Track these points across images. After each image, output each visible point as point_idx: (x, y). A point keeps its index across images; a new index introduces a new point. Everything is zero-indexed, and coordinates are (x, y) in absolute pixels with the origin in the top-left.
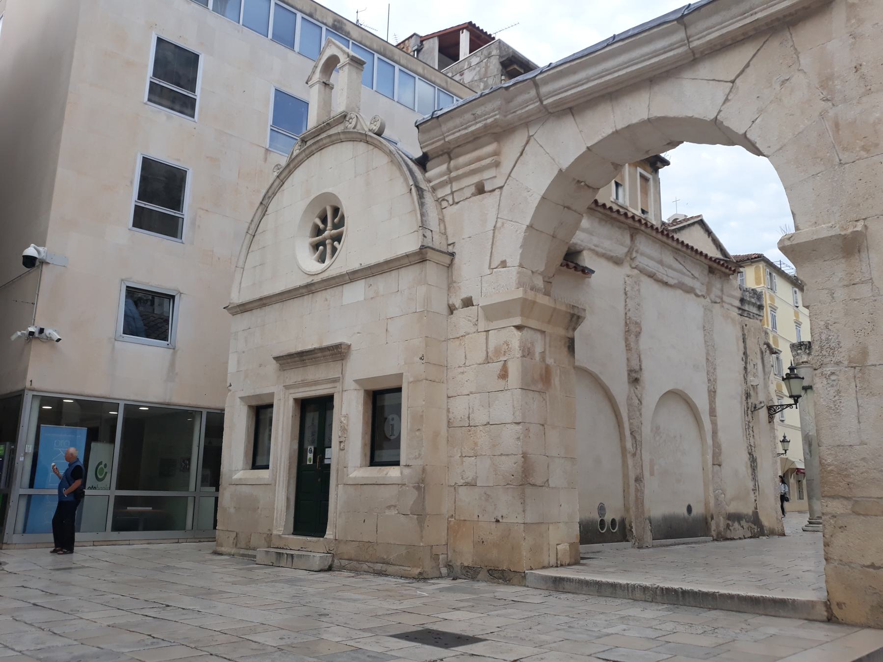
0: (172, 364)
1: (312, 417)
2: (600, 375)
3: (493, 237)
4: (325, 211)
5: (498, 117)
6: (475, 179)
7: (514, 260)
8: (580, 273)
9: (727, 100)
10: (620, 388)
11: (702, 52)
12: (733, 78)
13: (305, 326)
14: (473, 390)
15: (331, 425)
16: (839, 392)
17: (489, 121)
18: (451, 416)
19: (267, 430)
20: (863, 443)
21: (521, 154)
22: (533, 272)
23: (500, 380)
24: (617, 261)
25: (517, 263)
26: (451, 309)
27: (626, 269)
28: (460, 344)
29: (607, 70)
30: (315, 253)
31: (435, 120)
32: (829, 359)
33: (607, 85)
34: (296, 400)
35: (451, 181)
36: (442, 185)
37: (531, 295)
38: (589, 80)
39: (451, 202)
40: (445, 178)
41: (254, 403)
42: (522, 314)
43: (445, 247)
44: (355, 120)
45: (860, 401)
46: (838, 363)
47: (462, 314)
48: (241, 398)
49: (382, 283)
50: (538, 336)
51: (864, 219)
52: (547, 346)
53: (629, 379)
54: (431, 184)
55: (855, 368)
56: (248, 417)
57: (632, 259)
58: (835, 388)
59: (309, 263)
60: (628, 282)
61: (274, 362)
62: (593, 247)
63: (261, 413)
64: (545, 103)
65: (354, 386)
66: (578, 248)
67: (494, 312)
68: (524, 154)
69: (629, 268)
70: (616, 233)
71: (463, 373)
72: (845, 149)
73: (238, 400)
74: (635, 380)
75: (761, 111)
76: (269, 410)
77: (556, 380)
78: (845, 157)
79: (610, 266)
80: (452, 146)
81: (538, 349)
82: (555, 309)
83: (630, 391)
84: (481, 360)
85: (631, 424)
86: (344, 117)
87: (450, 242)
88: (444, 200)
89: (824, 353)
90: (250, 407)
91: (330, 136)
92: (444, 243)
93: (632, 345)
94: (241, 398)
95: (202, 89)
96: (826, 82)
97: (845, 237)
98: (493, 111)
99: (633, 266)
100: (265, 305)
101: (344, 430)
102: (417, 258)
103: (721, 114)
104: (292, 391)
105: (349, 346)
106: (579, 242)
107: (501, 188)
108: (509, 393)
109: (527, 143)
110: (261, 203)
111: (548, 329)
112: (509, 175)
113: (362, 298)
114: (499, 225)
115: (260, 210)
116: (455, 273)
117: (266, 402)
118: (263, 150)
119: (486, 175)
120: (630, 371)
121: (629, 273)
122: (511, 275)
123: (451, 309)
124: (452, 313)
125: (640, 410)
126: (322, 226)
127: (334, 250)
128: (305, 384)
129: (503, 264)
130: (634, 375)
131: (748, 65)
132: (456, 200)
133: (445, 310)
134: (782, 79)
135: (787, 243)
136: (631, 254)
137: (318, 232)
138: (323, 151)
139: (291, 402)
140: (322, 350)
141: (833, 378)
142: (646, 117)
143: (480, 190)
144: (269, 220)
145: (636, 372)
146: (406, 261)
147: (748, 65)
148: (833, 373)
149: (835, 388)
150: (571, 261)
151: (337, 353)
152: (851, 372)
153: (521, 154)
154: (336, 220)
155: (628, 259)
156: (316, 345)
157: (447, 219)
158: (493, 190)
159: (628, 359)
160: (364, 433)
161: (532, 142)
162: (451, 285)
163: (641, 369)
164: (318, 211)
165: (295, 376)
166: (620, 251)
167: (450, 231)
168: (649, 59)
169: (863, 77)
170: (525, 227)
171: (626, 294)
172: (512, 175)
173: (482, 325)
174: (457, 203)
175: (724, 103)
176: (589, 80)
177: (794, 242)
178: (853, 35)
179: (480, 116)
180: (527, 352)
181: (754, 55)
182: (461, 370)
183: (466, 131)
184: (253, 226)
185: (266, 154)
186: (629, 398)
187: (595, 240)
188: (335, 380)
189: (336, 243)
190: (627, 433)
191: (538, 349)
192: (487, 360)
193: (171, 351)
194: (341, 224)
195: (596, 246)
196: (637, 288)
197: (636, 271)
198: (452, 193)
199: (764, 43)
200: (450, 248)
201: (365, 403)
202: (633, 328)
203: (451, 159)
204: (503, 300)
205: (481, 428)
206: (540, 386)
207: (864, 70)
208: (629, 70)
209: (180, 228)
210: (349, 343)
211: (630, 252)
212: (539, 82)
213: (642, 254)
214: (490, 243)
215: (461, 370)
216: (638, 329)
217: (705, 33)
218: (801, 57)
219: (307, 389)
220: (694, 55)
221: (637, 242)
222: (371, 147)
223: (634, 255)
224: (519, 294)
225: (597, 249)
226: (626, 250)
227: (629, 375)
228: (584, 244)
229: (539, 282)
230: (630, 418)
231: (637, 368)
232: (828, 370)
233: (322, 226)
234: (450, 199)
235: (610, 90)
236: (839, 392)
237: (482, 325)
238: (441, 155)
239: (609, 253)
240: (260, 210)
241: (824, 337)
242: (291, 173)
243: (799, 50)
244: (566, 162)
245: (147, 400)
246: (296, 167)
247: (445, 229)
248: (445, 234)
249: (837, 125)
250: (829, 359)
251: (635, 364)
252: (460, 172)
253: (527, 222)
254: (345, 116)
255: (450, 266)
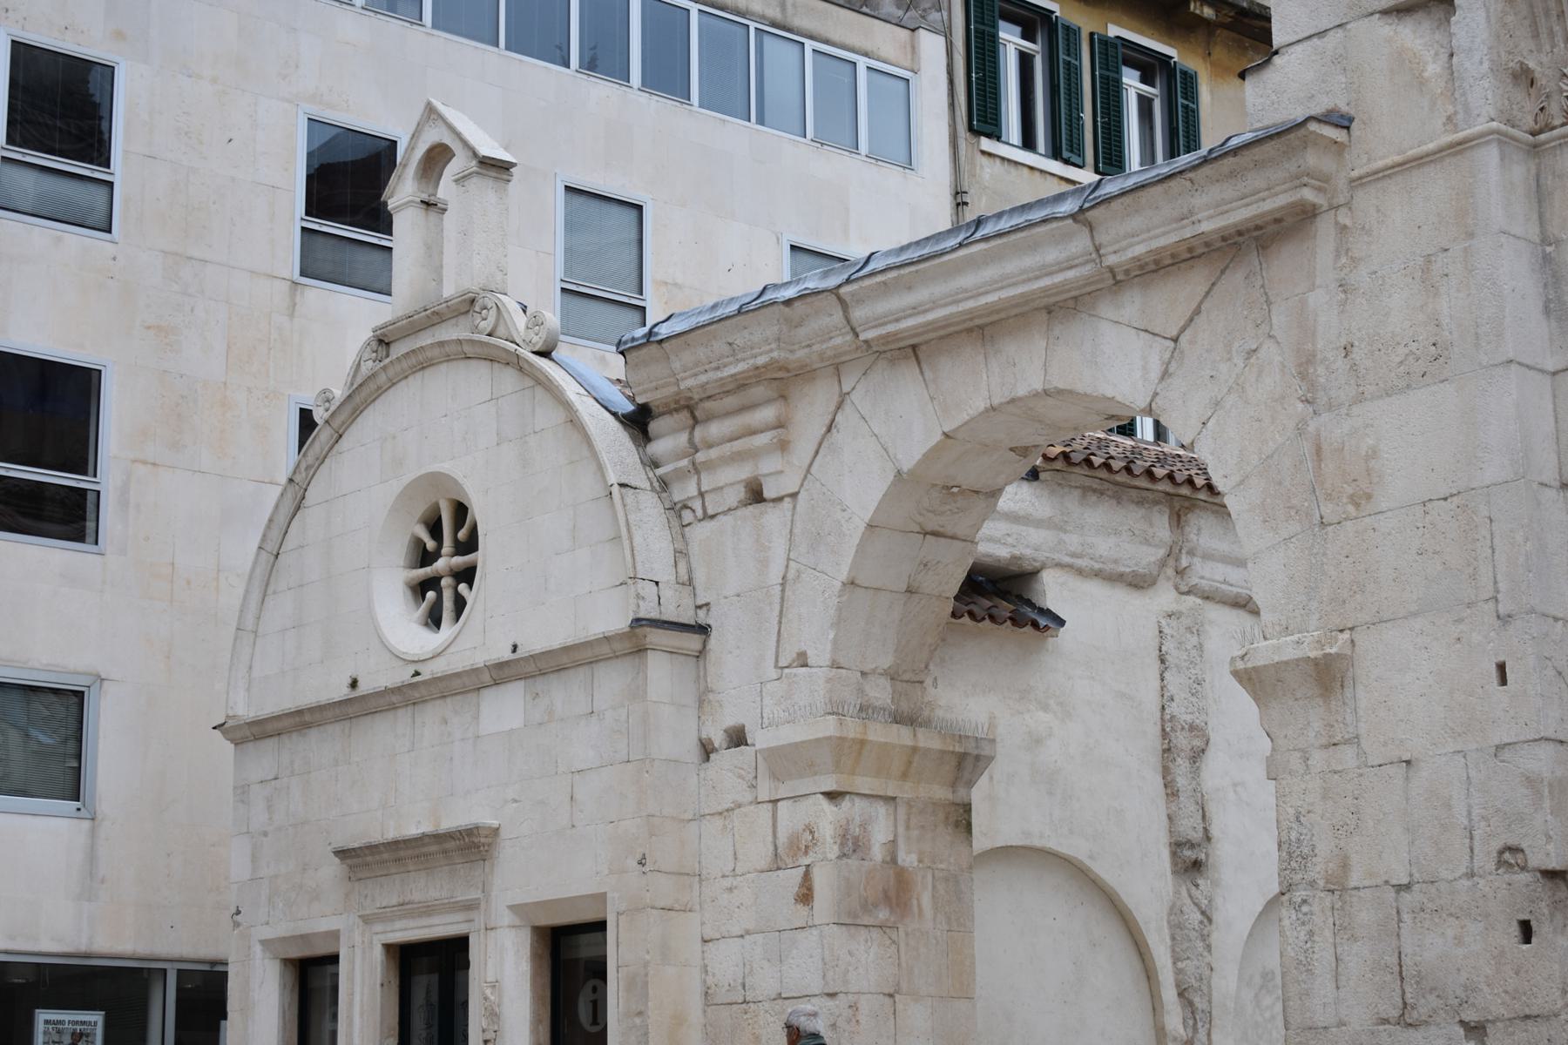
0: (92, 857)
1: (425, 986)
2: (1088, 862)
3: (782, 599)
4: (436, 510)
5: (775, 354)
6: (744, 472)
7: (820, 655)
8: (1028, 629)
9: (1165, 374)
10: (1148, 888)
11: (1127, 272)
12: (1174, 333)
13: (406, 783)
14: (751, 926)
15: (465, 1004)
16: (1311, 933)
17: (761, 360)
18: (710, 981)
19: (328, 1016)
20: (1341, 1024)
21: (829, 430)
22: (863, 674)
23: (800, 906)
24: (1138, 582)
25: (826, 659)
26: (707, 750)
27: (1164, 598)
28: (725, 827)
29: (966, 291)
30: (418, 606)
31: (654, 347)
32: (1300, 876)
33: (971, 314)
34: (388, 948)
35: (696, 469)
36: (681, 475)
37: (853, 729)
38: (935, 305)
39: (700, 513)
40: (685, 462)
41: (296, 953)
42: (837, 767)
43: (691, 612)
44: (493, 312)
45: (1339, 950)
46: (1312, 884)
47: (727, 759)
48: (264, 943)
49: (564, 694)
50: (881, 810)
51: (1351, 629)
52: (901, 830)
53: (1174, 864)
54: (660, 471)
55: (1333, 892)
56: (283, 986)
57: (1180, 572)
58: (1307, 928)
59: (405, 631)
60: (1166, 630)
61: (337, 860)
62: (1067, 560)
63: (311, 978)
64: (862, 337)
65: (507, 918)
66: (1027, 567)
67: (785, 762)
68: (834, 431)
69: (1174, 593)
70: (1132, 517)
71: (730, 890)
72: (1329, 497)
73: (258, 949)
74: (1190, 862)
75: (1217, 404)
76: (330, 969)
77: (925, 898)
78: (1328, 510)
79: (1120, 596)
80: (696, 397)
81: (880, 835)
82: (915, 749)
83: (1177, 892)
84: (763, 864)
85: (1179, 972)
86: (469, 305)
87: (699, 602)
88: (686, 507)
89: (1293, 864)
90: (287, 962)
91: (441, 344)
92: (688, 602)
93: (1182, 782)
94: (264, 943)
95: (126, 152)
96: (1305, 364)
97: (1315, 662)
98: (766, 341)
99: (1185, 589)
100: (307, 726)
101: (493, 1015)
102: (627, 646)
103: (1157, 399)
104: (378, 928)
105: (496, 831)
106: (1028, 552)
107: (794, 495)
108: (815, 932)
109: (839, 407)
110: (291, 480)
111: (905, 791)
112: (808, 471)
113: (517, 723)
114: (791, 575)
115: (289, 495)
116: (711, 670)
117: (321, 950)
118: (285, 286)
119: (767, 465)
120: (1177, 846)
121: (1174, 607)
122: (813, 685)
123: (707, 750)
124: (708, 759)
125: (1204, 938)
126: (431, 545)
127: (460, 604)
128: (406, 909)
129: (802, 661)
130: (1188, 854)
131: (1197, 311)
132: (710, 512)
133: (694, 753)
134: (1247, 347)
135: (1240, 665)
136: (1177, 560)
137: (425, 557)
138: (427, 372)
139: (378, 954)
140: (438, 838)
141: (1305, 909)
142: (1039, 387)
143: (756, 495)
144: (312, 516)
145: (1192, 846)
146: (605, 649)
147: (1197, 311)
148: (1304, 901)
149: (1307, 928)
150: (1000, 597)
151: (470, 846)
152: (1328, 899)
153: (829, 430)
154: (462, 534)
155: (1170, 572)
156: (426, 828)
157: (694, 549)
158: (780, 499)
159: (1170, 817)
160: (536, 1021)
161: (847, 407)
162: (703, 699)
163: (1209, 839)
164: (421, 509)
165: (386, 893)
166: (1144, 557)
167: (700, 577)
168: (1037, 278)
169: (1354, 367)
170: (838, 585)
171: (1163, 661)
172: (813, 470)
173: (765, 791)
174: (713, 517)
175: (1162, 378)
176: (935, 305)
177: (1250, 665)
178: (1343, 286)
179: (743, 349)
180: (852, 844)
181: (1208, 293)
182: (727, 883)
183: (719, 374)
184: (275, 534)
185: (293, 295)
186: (1175, 910)
187: (1073, 541)
188: (470, 906)
189: (462, 587)
190: (1169, 994)
191: (880, 835)
192: (777, 864)
193: (86, 824)
194: (469, 545)
195: (1073, 555)
196: (1194, 640)
197: (1192, 600)
198: (702, 495)
199: (1223, 272)
200: (702, 613)
201: (536, 956)
202: (1182, 740)
203: (696, 421)
204: (798, 739)
205: (767, 1005)
206: (883, 914)
207: (1357, 354)
208: (1004, 294)
209: (90, 515)
210: (495, 823)
211: (1173, 553)
212: (848, 299)
213: (1208, 557)
214: (776, 612)
215: (727, 883)
216: (1197, 743)
217: (1124, 243)
218: (1274, 308)
219: (412, 923)
220: (1114, 277)
221: (1191, 531)
222: (529, 382)
223: (1184, 562)
224: (828, 727)
225: (1079, 562)
226: (1162, 552)
227: (1174, 854)
228: (1042, 556)
229: (880, 692)
230: (1176, 959)
231: (1197, 836)
232: (1299, 895)
233: (431, 545)
234: (697, 505)
235: (978, 322)
236: (1311, 933)
237: (765, 791)
238: (676, 410)
239: (1109, 567)
240: (289, 495)
241: (1294, 835)
242: (356, 413)
243: (1272, 299)
244: (910, 454)
245: (36, 949)
246: (367, 404)
247: (690, 571)
248: (690, 582)
249: (1318, 450)
250: (1300, 876)
251: (1189, 827)
252: (714, 453)
253: (843, 575)
254: (473, 301)
255: (701, 654)
